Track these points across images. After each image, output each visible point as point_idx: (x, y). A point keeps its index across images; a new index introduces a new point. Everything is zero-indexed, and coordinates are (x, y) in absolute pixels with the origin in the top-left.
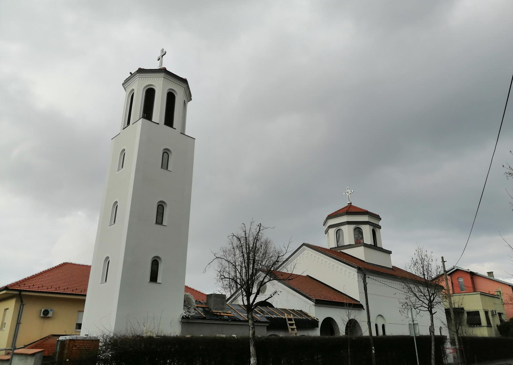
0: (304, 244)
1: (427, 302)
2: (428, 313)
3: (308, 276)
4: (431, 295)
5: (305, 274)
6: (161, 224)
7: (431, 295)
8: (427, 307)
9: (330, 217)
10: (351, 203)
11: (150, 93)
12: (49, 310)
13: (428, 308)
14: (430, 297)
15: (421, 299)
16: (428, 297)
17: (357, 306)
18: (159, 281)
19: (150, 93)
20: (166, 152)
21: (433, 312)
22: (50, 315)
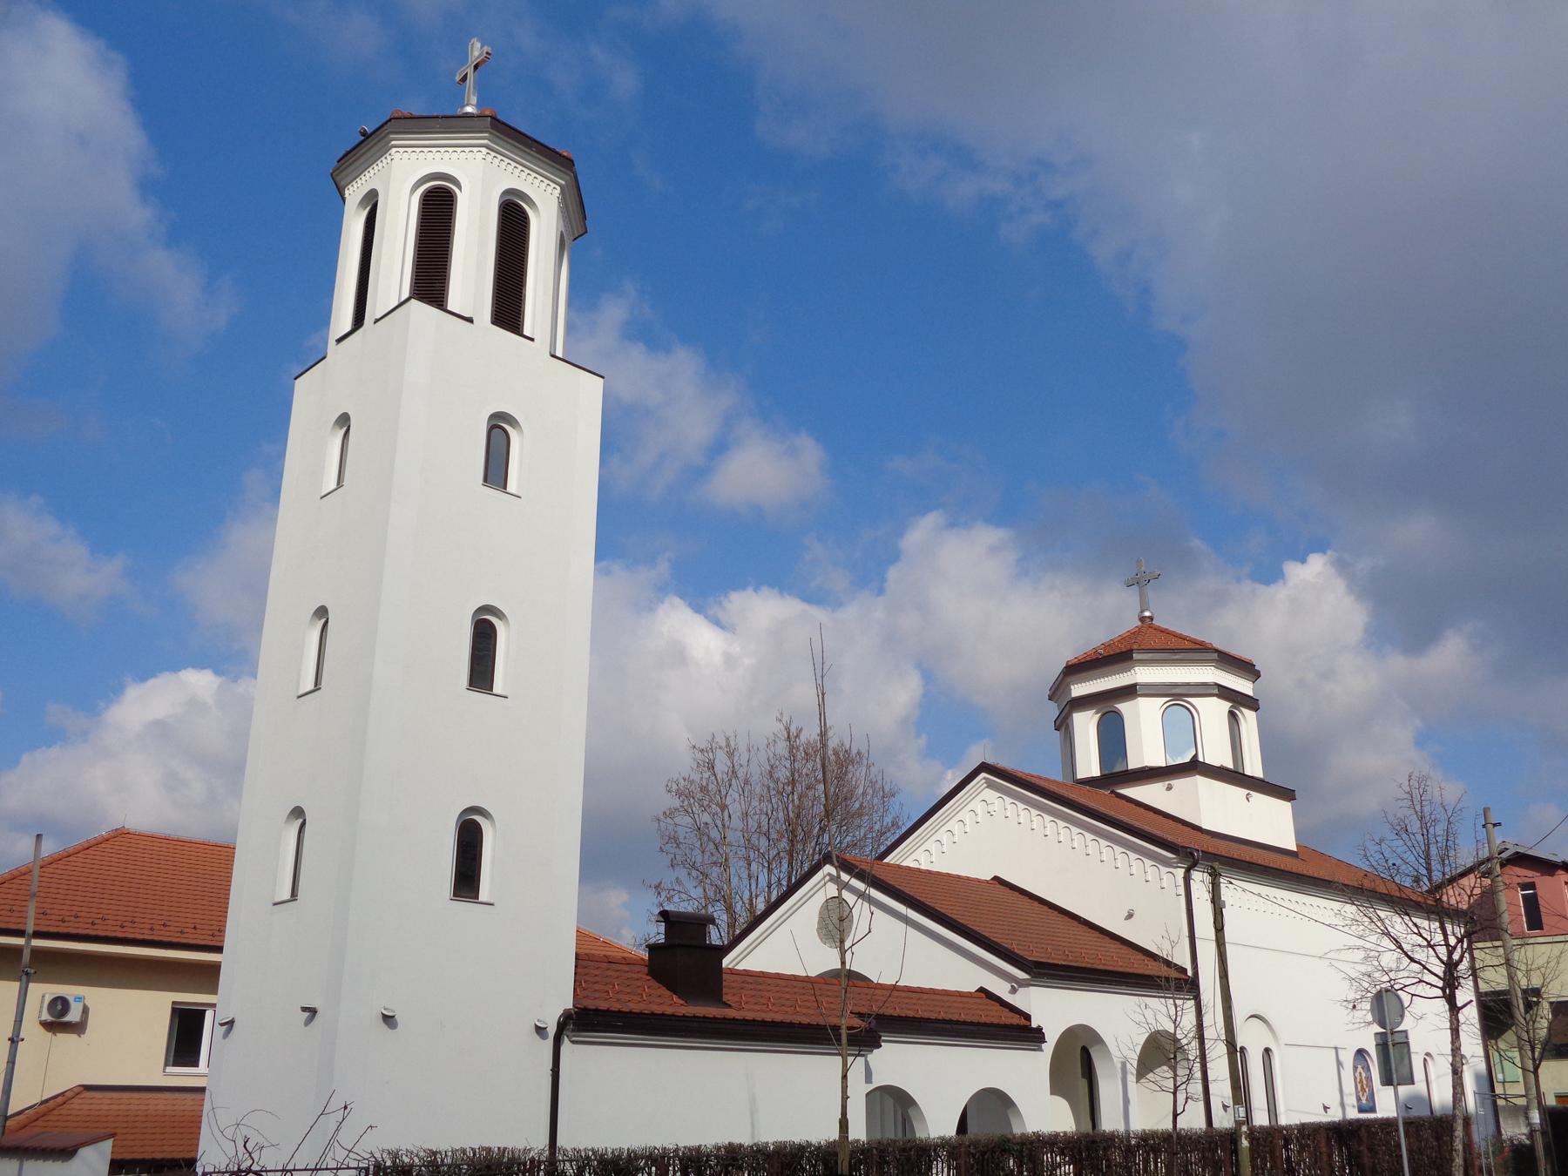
0: (984, 767)
1: (1439, 969)
2: (1442, 1005)
3: (996, 879)
4: (1452, 941)
5: (983, 872)
6: (502, 484)
7: (1452, 941)
8: (1440, 984)
9: (1076, 669)
10: (852, 762)
11: (438, 206)
12: (71, 1000)
13: (1443, 989)
14: (1450, 954)
15: (1416, 956)
16: (1442, 951)
17: (1185, 984)
18: (484, 895)
19: (438, 206)
20: (499, 428)
21: (1459, 1004)
22: (73, 1016)
